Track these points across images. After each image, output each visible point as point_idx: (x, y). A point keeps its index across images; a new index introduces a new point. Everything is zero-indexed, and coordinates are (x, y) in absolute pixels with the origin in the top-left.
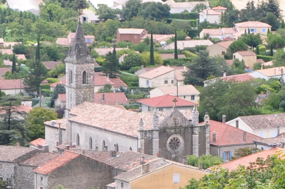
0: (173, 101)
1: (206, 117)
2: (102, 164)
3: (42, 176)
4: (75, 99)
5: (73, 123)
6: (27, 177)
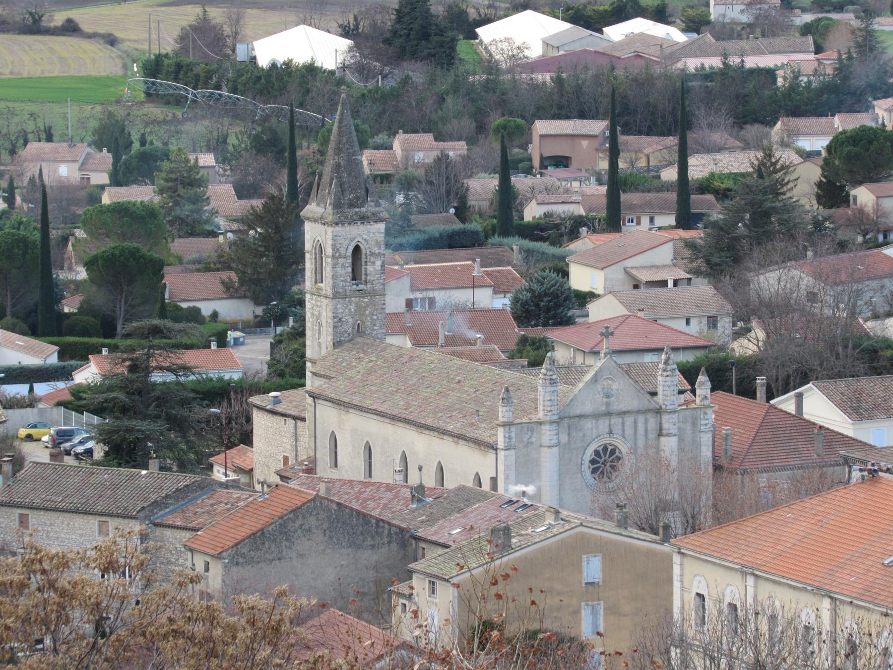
0: (602, 334)
1: (702, 384)
2: (381, 524)
3: (208, 559)
4: (330, 330)
5: (320, 401)
6: (177, 560)
